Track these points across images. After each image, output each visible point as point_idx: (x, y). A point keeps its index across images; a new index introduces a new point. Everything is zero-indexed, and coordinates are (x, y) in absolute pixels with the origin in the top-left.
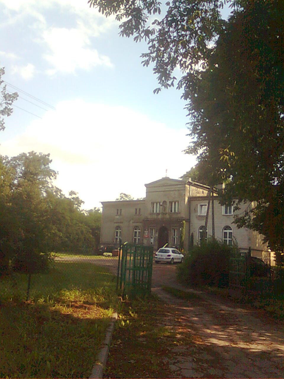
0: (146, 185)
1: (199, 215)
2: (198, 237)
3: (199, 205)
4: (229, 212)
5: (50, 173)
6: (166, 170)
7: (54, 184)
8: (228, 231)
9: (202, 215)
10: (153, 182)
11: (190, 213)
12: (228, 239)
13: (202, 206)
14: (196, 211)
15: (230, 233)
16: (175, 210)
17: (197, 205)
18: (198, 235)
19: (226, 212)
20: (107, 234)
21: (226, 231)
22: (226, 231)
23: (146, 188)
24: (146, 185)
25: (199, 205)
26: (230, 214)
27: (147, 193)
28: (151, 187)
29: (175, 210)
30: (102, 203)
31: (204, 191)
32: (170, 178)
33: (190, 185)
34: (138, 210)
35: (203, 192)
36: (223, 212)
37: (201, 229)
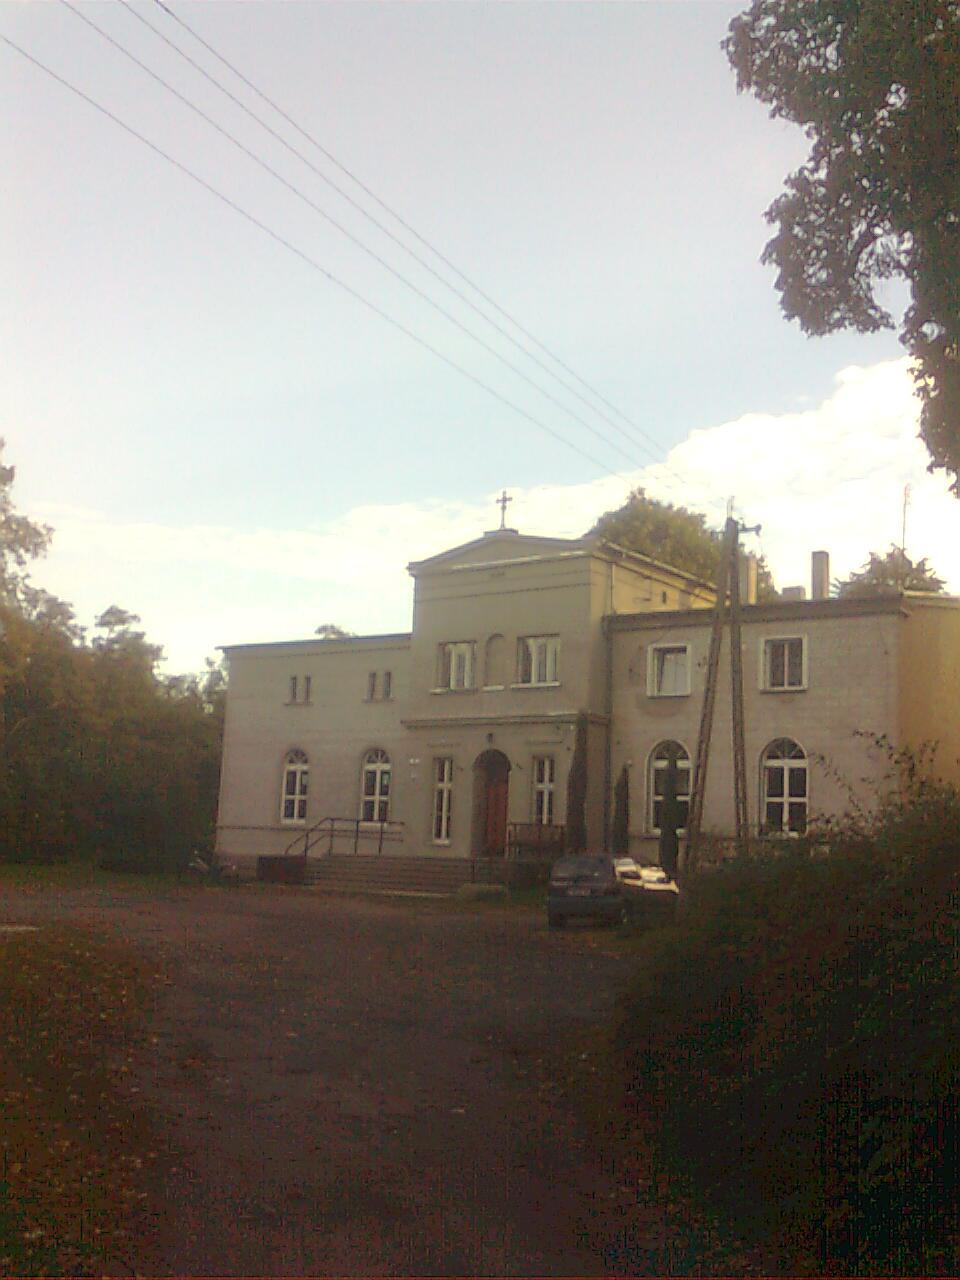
0: (416, 569)
1: (649, 694)
2: (648, 793)
3: (650, 649)
4: (791, 675)
5: (155, 653)
6: (505, 500)
7: (34, 584)
8: (787, 764)
9: (663, 694)
10: (451, 551)
11: (609, 687)
12: (786, 799)
13: (662, 653)
14: (635, 674)
15: (798, 776)
16: (460, 681)
17: (642, 649)
18: (648, 787)
19: (776, 680)
20: (248, 817)
21: (775, 763)
22: (775, 763)
23: (413, 580)
24: (416, 569)
25: (650, 649)
26: (542, 685)
27: (415, 602)
28: (434, 577)
29: (460, 681)
30: (226, 650)
31: (670, 592)
32: (524, 531)
33: (610, 563)
34: (301, 683)
35: (664, 595)
36: (761, 681)
37: (660, 758)
